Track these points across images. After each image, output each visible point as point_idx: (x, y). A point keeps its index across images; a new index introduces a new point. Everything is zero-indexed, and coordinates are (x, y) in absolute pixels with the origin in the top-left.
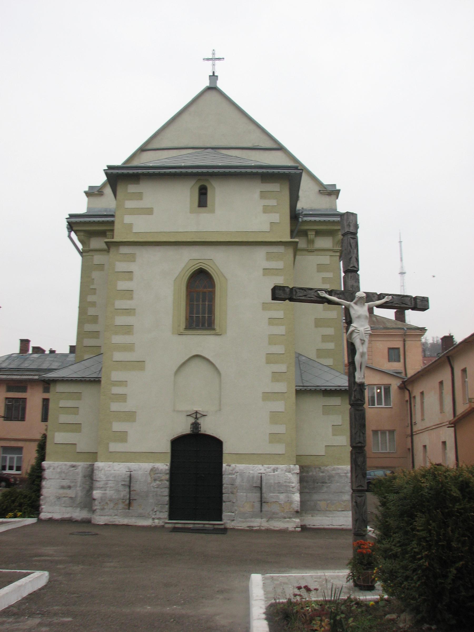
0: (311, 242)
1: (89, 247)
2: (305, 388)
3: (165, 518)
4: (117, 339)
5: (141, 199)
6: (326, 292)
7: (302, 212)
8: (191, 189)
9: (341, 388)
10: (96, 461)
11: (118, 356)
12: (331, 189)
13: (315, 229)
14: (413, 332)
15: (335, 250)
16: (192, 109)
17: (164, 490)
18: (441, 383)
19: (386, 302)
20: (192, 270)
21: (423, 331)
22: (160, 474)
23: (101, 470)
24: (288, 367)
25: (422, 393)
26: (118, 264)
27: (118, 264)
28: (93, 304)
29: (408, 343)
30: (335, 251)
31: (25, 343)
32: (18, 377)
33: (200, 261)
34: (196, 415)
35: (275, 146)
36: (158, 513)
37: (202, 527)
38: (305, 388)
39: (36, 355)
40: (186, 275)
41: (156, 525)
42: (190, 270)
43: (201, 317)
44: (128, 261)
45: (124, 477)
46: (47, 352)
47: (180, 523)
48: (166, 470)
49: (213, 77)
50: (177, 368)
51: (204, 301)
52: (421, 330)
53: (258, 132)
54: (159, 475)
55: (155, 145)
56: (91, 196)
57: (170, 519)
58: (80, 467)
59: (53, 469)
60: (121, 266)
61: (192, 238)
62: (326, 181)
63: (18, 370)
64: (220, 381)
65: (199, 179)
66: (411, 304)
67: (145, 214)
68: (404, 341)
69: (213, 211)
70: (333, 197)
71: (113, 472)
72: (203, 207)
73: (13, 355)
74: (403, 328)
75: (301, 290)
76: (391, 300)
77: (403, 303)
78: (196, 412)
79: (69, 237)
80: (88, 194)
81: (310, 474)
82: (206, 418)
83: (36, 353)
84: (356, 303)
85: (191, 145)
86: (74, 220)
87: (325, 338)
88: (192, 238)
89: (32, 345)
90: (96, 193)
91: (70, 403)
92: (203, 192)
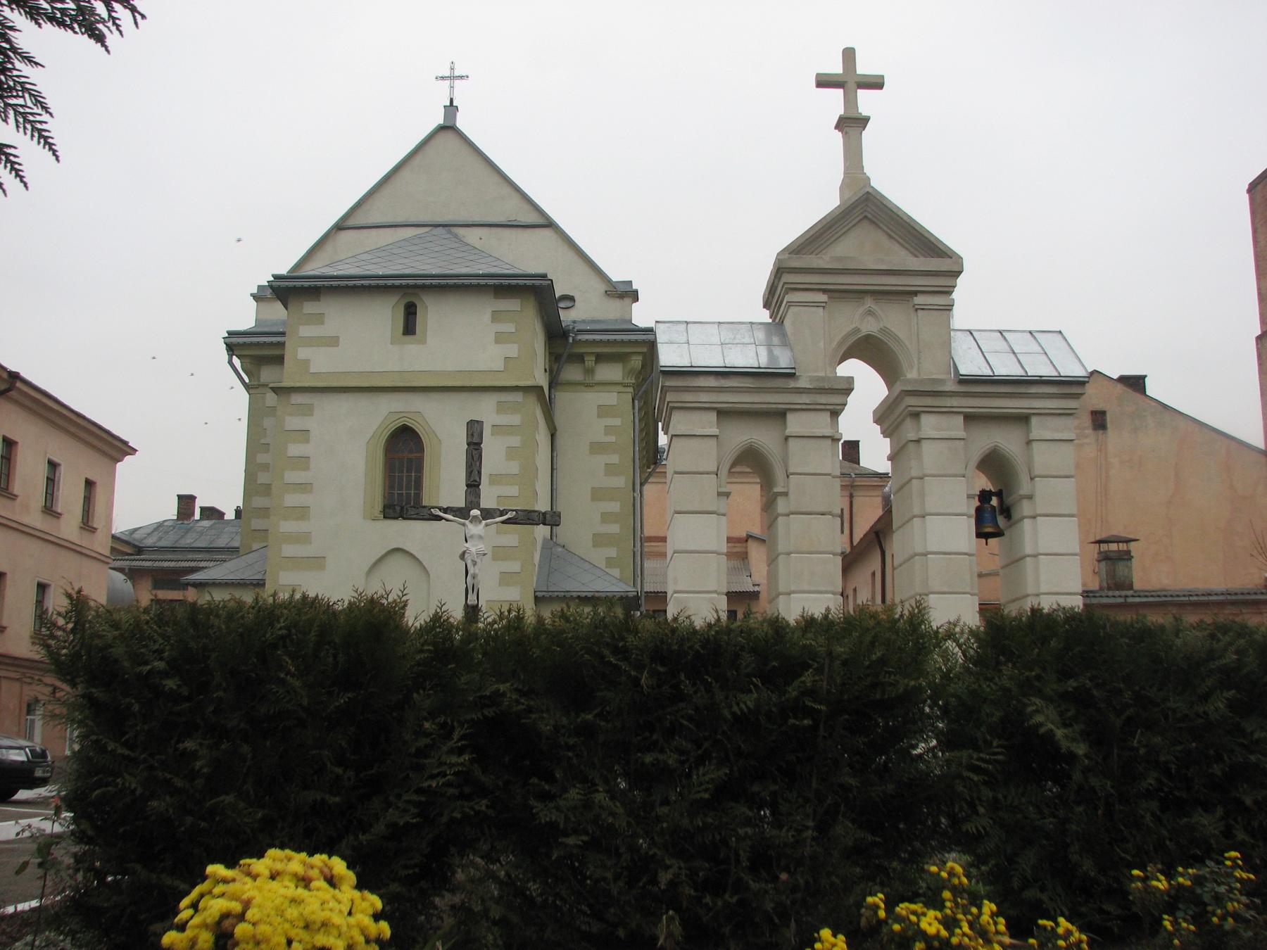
0: (589, 372)
1: (259, 381)
2: (550, 594)
4: (287, 526)
5: (323, 323)
6: (440, 510)
7: (574, 328)
9: (579, 594)
11: (289, 550)
12: (622, 288)
14: (866, 482)
16: (417, 160)
18: (874, 574)
19: (509, 519)
21: (884, 479)
24: (522, 566)
25: (855, 590)
26: (288, 418)
27: (288, 418)
28: (266, 467)
29: (857, 501)
30: (626, 386)
31: (186, 502)
32: (172, 564)
35: (541, 221)
38: (550, 594)
39: (206, 523)
40: (384, 434)
46: (230, 515)
49: (451, 109)
51: (409, 470)
52: (881, 478)
55: (358, 220)
60: (293, 422)
63: (173, 549)
64: (429, 581)
68: (851, 496)
69: (423, 342)
70: (627, 301)
72: (413, 334)
73: (166, 524)
74: (849, 473)
77: (529, 519)
79: (230, 363)
83: (208, 518)
84: (471, 522)
85: (413, 220)
86: (234, 340)
87: (606, 518)
89: (199, 504)
92: (410, 312)
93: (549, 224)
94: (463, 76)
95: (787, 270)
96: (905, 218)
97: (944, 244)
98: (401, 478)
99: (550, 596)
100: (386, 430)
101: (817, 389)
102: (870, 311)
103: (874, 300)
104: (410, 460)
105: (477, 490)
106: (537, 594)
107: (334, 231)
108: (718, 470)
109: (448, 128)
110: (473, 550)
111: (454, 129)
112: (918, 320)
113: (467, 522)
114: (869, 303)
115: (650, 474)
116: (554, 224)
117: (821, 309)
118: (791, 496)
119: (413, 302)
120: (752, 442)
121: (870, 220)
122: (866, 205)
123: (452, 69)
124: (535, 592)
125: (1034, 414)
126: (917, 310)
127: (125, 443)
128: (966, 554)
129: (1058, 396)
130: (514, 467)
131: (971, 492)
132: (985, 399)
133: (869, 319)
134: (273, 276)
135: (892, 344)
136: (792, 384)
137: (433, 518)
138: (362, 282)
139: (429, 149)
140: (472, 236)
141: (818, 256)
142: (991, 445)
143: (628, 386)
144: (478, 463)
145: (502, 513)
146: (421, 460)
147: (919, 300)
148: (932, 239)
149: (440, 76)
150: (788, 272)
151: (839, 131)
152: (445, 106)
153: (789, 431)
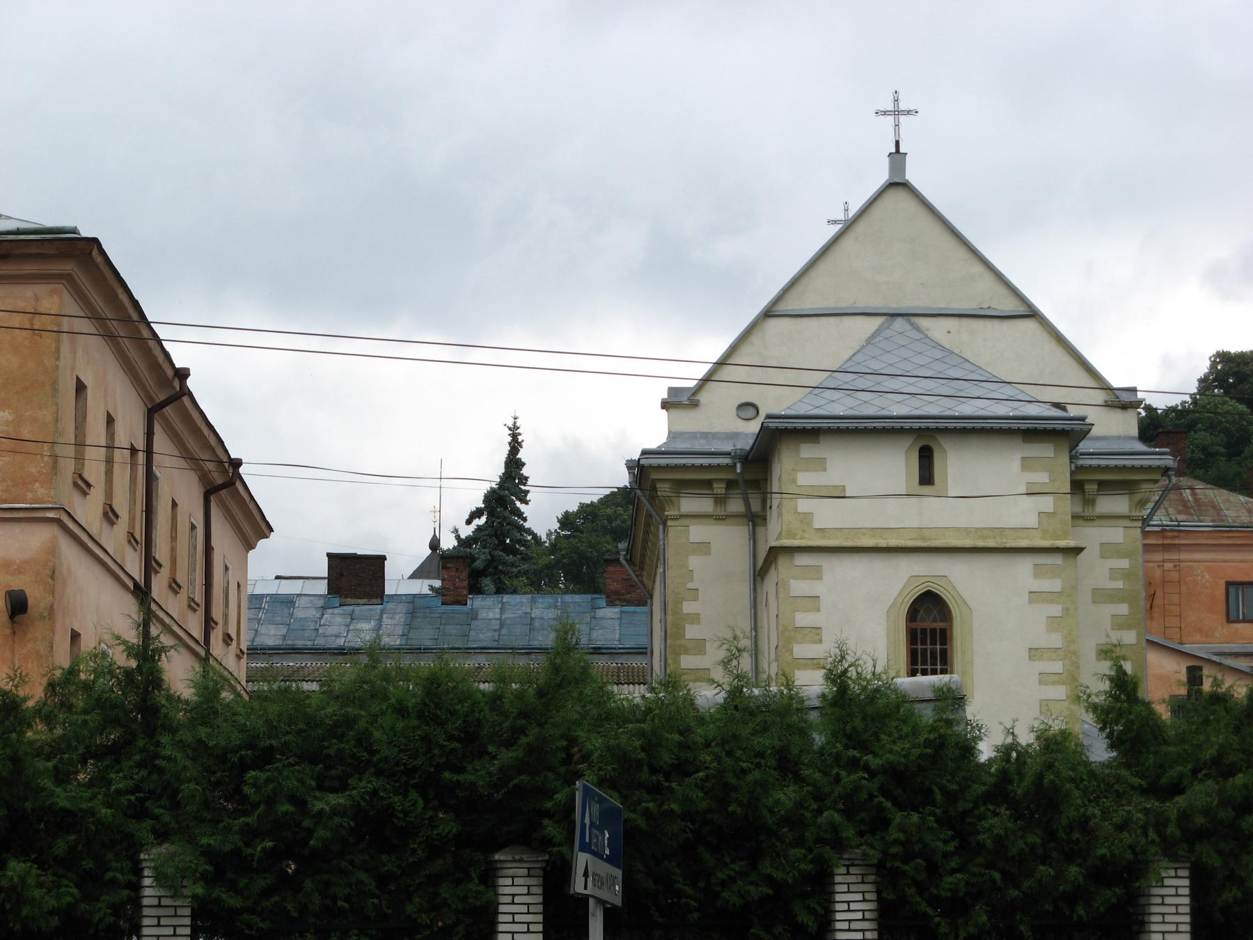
1: (679, 510)
8: (906, 452)
12: (1125, 397)
13: (1097, 480)
15: (1133, 517)
20: (917, 593)
33: (927, 579)
35: (1022, 310)
44: (811, 579)
49: (897, 156)
56: (675, 407)
60: (800, 587)
62: (1116, 382)
80: (665, 405)
90: (685, 403)
92: (926, 458)
93: (1032, 314)
100: (909, 596)
104: (933, 631)
107: (761, 320)
109: (898, 184)
116: (1038, 314)
130: (1056, 640)
143: (1136, 520)
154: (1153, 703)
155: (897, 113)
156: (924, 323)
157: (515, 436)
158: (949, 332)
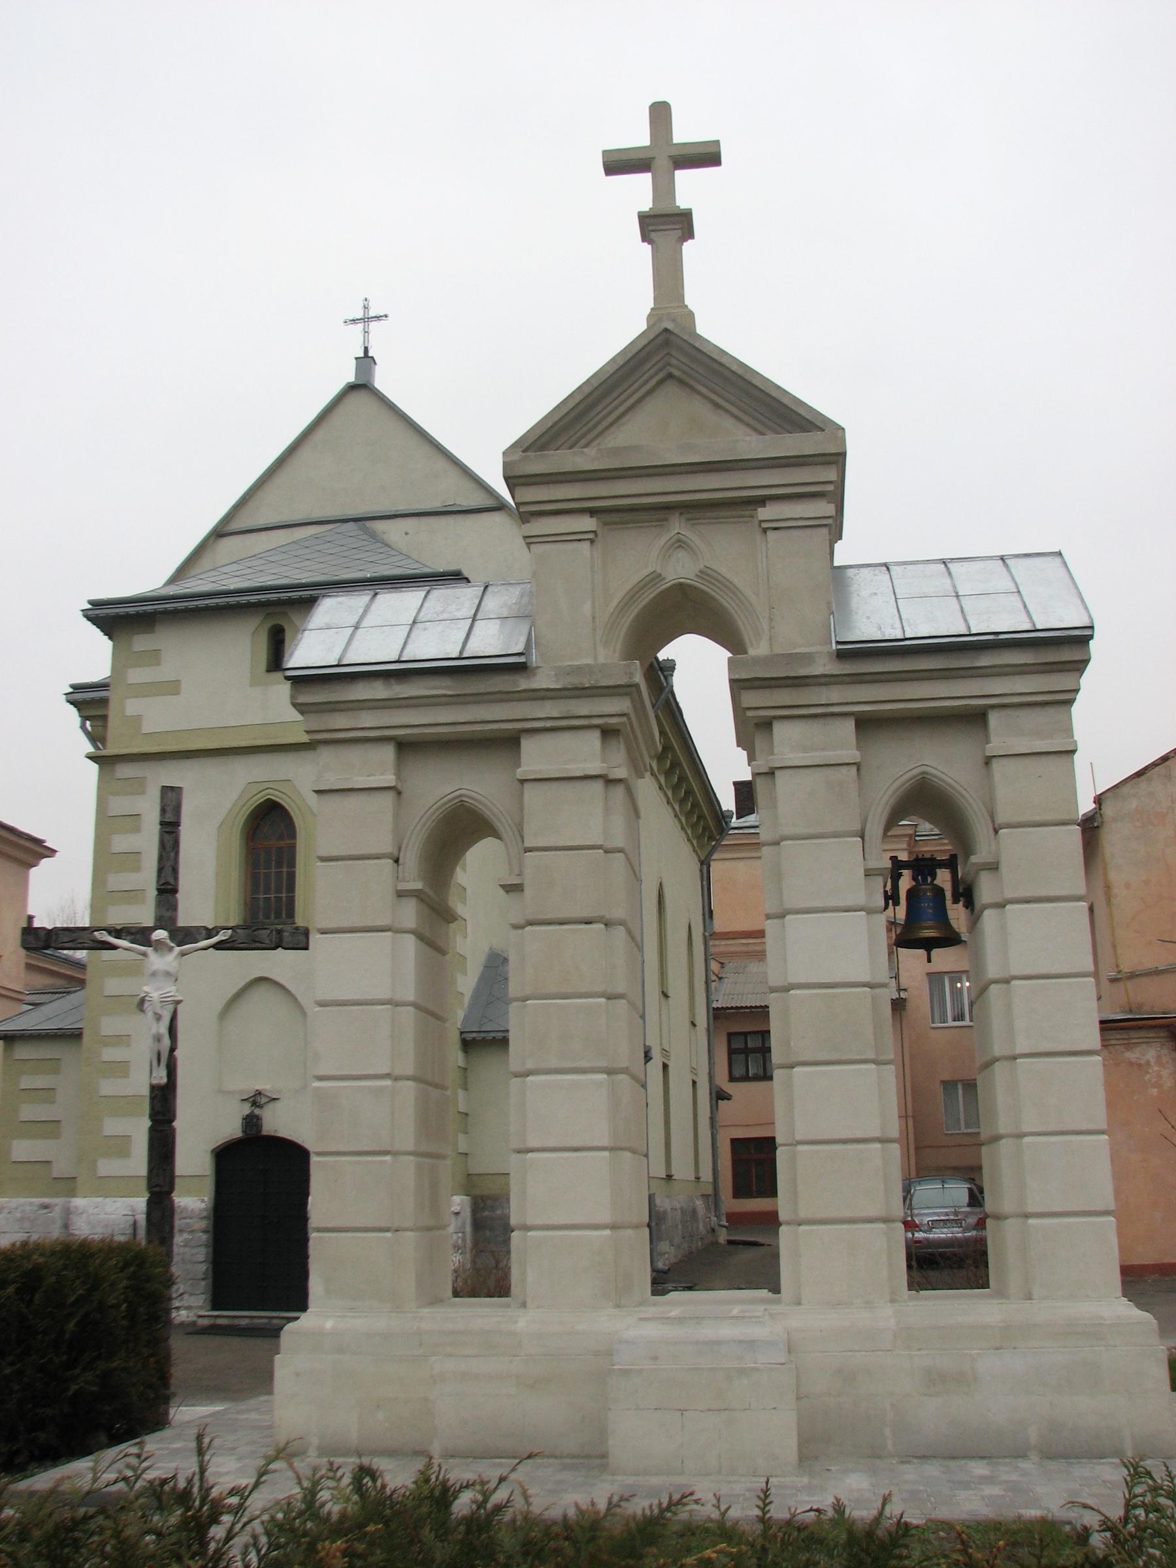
2: (483, 1035)
3: (201, 1308)
5: (158, 663)
10: (74, 1196)
17: (196, 1250)
22: (191, 1218)
23: (82, 1213)
33: (267, 785)
34: (256, 1100)
35: (489, 502)
36: (186, 1296)
37: (264, 1324)
38: (483, 1035)
41: (183, 1320)
42: (248, 805)
43: (273, 899)
45: (123, 1226)
47: (225, 1317)
48: (201, 1210)
49: (366, 361)
50: (224, 1002)
51: (279, 864)
53: (453, 474)
54: (188, 1221)
57: (214, 1308)
58: (57, 1208)
59: (9, 1213)
61: (255, 739)
65: (268, 614)
66: (271, 940)
67: (163, 695)
71: (102, 1216)
75: (67, 932)
76: (231, 937)
78: (259, 1093)
81: (499, 1212)
82: (278, 1104)
84: (156, 950)
88: (255, 739)
91: (39, 1082)
94: (381, 316)
95: (522, 480)
96: (734, 368)
97: (810, 407)
98: (267, 876)
99: (484, 1038)
101: (569, 689)
102: (679, 541)
103: (688, 520)
105: (171, 897)
106: (465, 1035)
108: (400, 851)
110: (155, 996)
111: (370, 389)
112: (767, 549)
113: (149, 950)
114: (677, 526)
115: (713, 850)
117: (587, 545)
118: (528, 891)
119: (281, 626)
120: (461, 796)
121: (681, 382)
122: (668, 354)
123: (366, 307)
124: (462, 1033)
125: (993, 707)
126: (765, 531)
127: (39, 842)
128: (864, 985)
129: (1040, 668)
131: (874, 864)
132: (895, 684)
133: (680, 555)
134: (90, 602)
135: (725, 600)
136: (523, 683)
137: (100, 946)
138: (207, 602)
139: (336, 419)
140: (392, 531)
141: (575, 449)
142: (915, 772)
144: (172, 854)
145: (210, 933)
146: (293, 848)
147: (764, 513)
148: (785, 401)
149: (351, 318)
150: (523, 485)
151: (649, 244)
152: (356, 358)
153: (523, 771)
154: (285, 931)
155: (366, 320)
156: (379, 526)
157: (661, 884)
158: (406, 534)
